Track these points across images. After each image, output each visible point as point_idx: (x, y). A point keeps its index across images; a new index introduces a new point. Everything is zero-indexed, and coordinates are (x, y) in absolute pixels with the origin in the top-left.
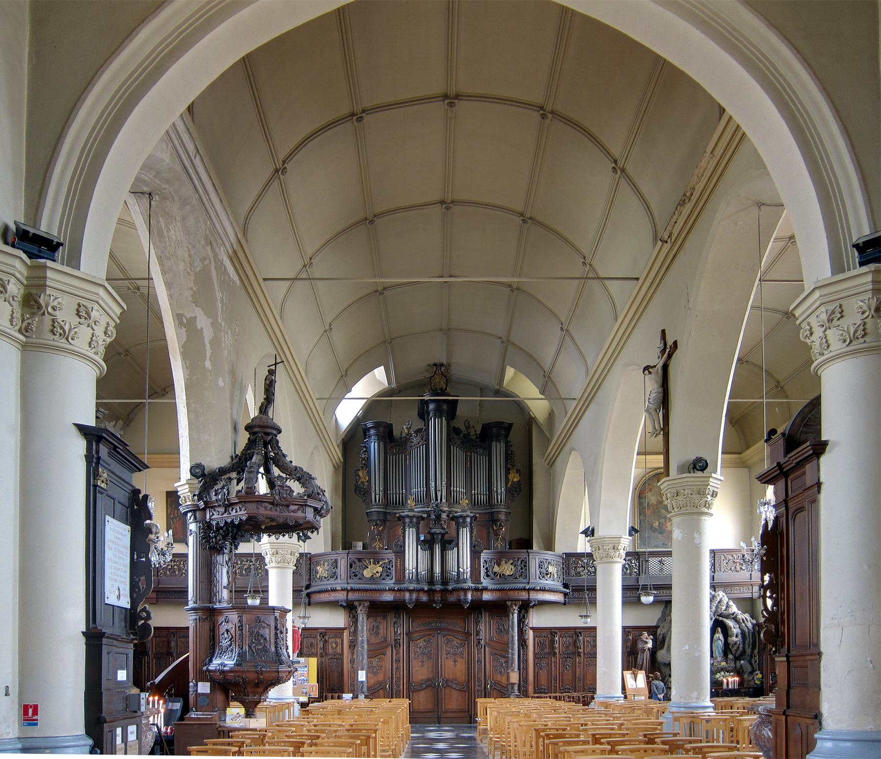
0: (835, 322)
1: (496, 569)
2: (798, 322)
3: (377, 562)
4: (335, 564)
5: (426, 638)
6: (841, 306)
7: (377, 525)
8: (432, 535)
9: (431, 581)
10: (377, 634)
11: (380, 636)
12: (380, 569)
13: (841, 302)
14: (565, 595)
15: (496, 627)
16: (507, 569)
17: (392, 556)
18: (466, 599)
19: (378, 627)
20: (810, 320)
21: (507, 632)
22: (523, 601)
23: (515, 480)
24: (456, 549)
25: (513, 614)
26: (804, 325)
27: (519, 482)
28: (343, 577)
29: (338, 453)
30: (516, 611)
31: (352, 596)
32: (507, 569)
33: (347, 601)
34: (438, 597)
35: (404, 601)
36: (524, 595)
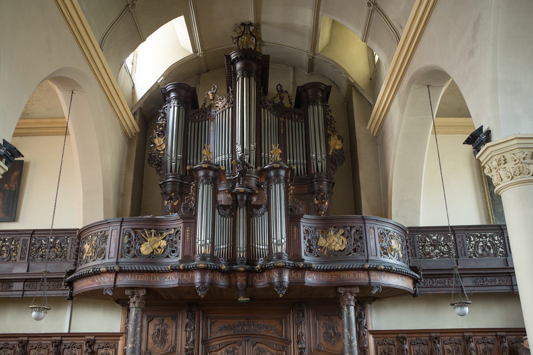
0: (502, 166)
1: (322, 242)
2: (482, 165)
3: (159, 233)
4: (104, 238)
5: (230, 348)
6: (504, 157)
7: (171, 198)
8: (234, 195)
9: (232, 260)
10: (163, 341)
11: (167, 345)
12: (164, 243)
13: (504, 154)
14: (415, 282)
15: (323, 330)
16: (336, 242)
17: (180, 225)
18: (281, 282)
19: (165, 333)
20: (489, 163)
21: (339, 336)
22: (362, 287)
23: (337, 147)
24: (266, 214)
25: (348, 306)
26: (487, 166)
27: (341, 149)
28: (112, 255)
29: (132, 123)
30: (352, 303)
31: (123, 281)
32: (336, 242)
33: (115, 288)
34: (240, 280)
35: (193, 285)
36: (362, 278)
